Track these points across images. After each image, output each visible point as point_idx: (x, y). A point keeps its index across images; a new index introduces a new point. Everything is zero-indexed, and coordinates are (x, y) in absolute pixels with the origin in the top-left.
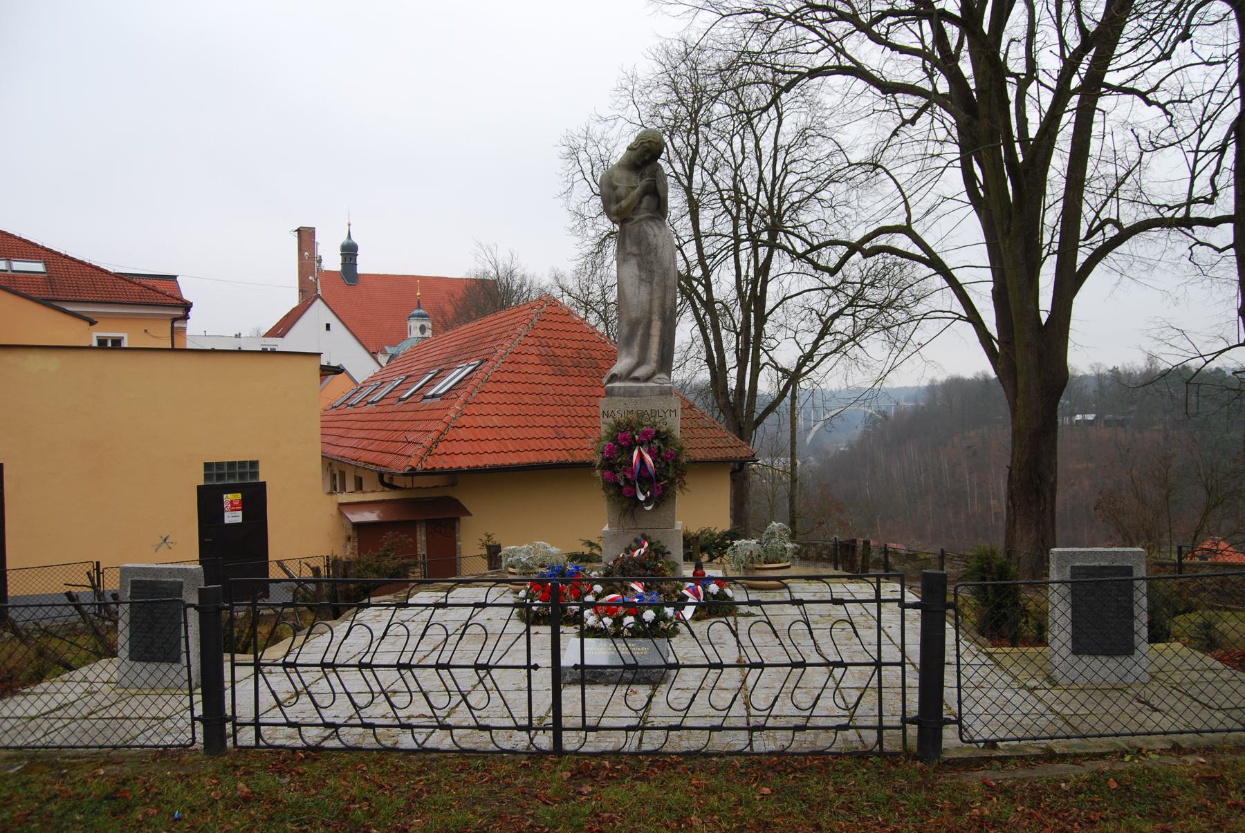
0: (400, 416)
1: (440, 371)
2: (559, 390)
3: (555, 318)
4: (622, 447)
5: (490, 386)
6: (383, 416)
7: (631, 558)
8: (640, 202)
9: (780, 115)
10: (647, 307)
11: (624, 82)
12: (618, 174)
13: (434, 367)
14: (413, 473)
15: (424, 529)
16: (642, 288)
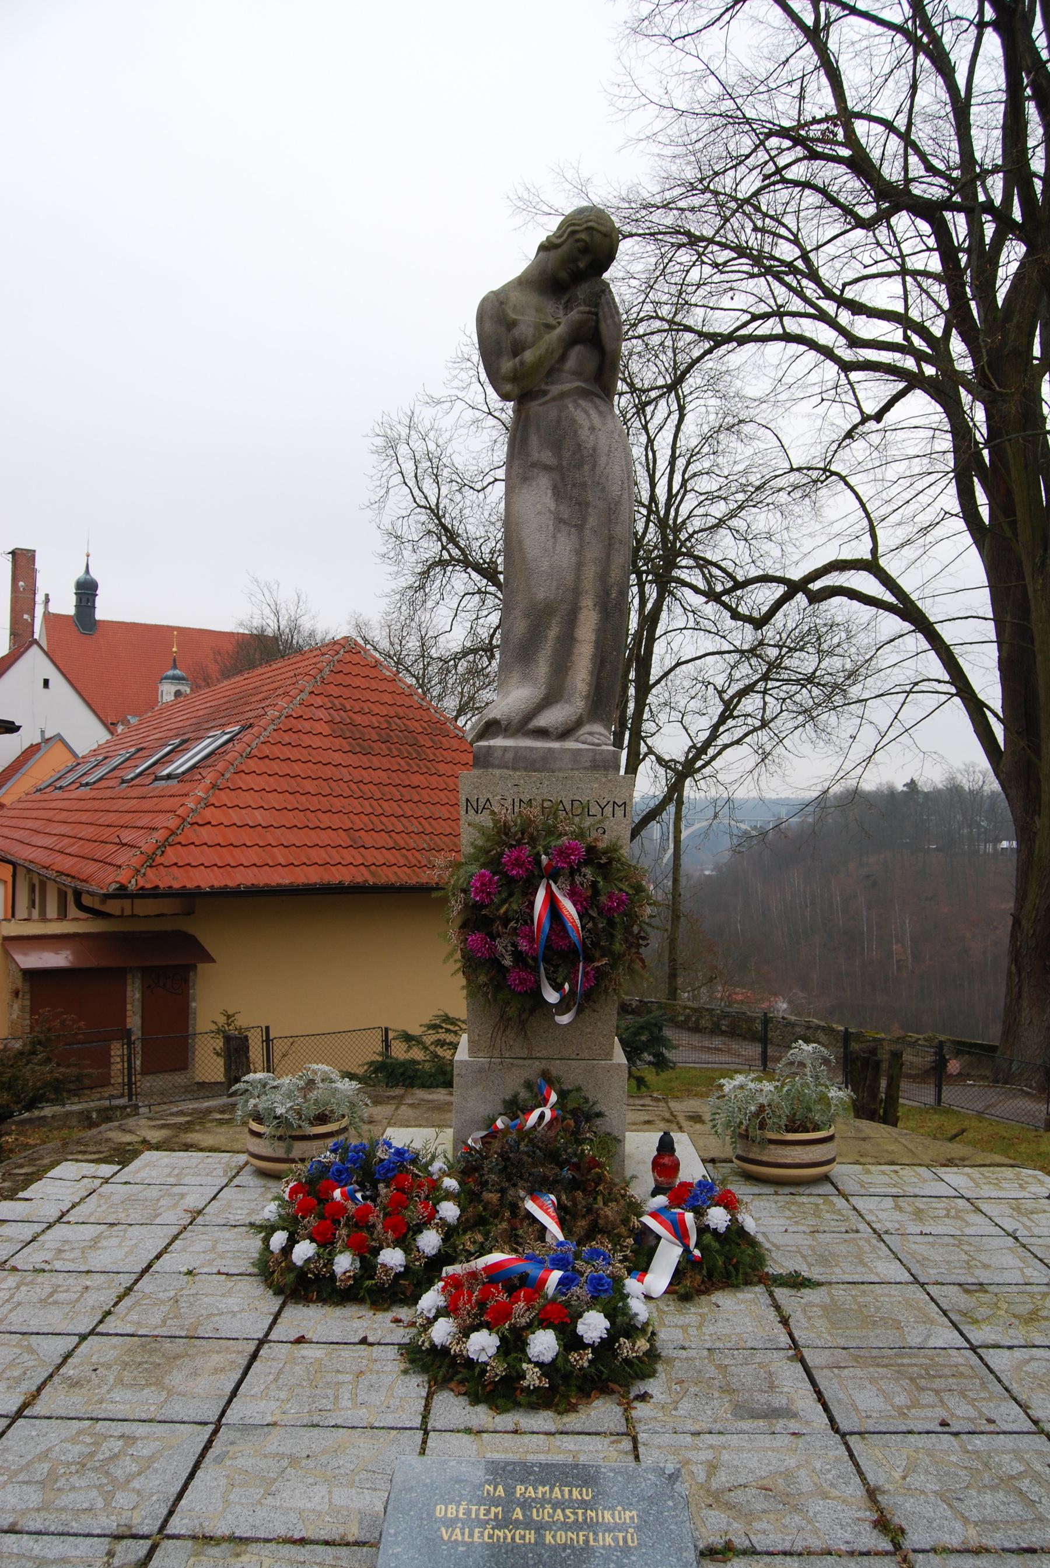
0: (120, 805)
1: (184, 742)
2: (358, 774)
3: (356, 670)
4: (510, 881)
5: (252, 764)
6: (96, 805)
7: (524, 1134)
8: (563, 358)
9: (681, 409)
10: (570, 578)
11: (466, 349)
12: (515, 297)
13: (177, 736)
14: (122, 892)
15: (138, 984)
16: (562, 538)
